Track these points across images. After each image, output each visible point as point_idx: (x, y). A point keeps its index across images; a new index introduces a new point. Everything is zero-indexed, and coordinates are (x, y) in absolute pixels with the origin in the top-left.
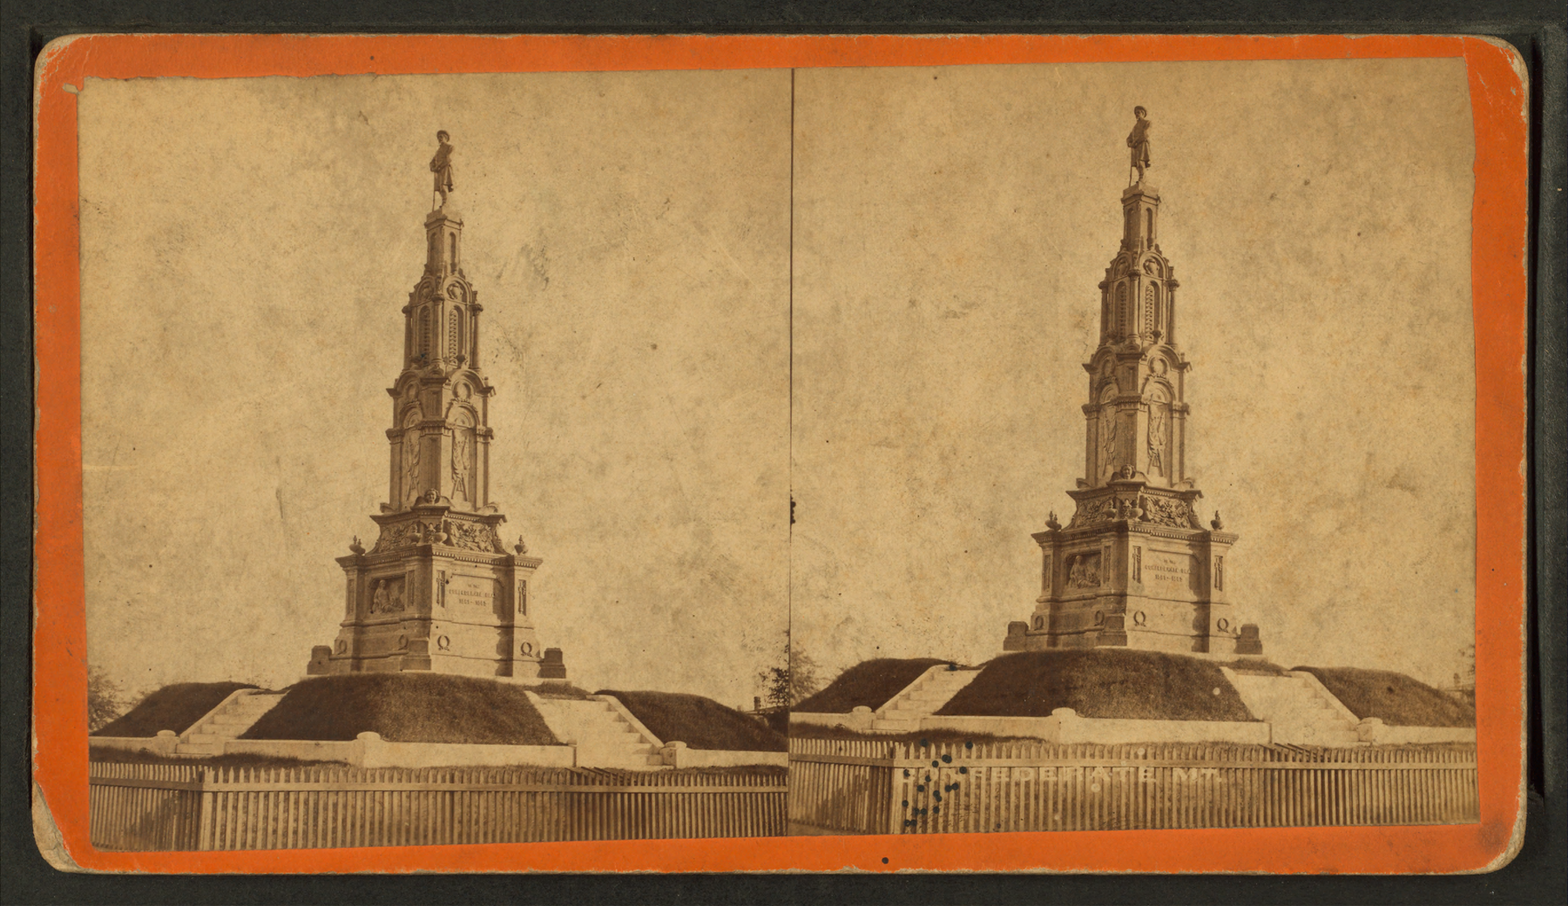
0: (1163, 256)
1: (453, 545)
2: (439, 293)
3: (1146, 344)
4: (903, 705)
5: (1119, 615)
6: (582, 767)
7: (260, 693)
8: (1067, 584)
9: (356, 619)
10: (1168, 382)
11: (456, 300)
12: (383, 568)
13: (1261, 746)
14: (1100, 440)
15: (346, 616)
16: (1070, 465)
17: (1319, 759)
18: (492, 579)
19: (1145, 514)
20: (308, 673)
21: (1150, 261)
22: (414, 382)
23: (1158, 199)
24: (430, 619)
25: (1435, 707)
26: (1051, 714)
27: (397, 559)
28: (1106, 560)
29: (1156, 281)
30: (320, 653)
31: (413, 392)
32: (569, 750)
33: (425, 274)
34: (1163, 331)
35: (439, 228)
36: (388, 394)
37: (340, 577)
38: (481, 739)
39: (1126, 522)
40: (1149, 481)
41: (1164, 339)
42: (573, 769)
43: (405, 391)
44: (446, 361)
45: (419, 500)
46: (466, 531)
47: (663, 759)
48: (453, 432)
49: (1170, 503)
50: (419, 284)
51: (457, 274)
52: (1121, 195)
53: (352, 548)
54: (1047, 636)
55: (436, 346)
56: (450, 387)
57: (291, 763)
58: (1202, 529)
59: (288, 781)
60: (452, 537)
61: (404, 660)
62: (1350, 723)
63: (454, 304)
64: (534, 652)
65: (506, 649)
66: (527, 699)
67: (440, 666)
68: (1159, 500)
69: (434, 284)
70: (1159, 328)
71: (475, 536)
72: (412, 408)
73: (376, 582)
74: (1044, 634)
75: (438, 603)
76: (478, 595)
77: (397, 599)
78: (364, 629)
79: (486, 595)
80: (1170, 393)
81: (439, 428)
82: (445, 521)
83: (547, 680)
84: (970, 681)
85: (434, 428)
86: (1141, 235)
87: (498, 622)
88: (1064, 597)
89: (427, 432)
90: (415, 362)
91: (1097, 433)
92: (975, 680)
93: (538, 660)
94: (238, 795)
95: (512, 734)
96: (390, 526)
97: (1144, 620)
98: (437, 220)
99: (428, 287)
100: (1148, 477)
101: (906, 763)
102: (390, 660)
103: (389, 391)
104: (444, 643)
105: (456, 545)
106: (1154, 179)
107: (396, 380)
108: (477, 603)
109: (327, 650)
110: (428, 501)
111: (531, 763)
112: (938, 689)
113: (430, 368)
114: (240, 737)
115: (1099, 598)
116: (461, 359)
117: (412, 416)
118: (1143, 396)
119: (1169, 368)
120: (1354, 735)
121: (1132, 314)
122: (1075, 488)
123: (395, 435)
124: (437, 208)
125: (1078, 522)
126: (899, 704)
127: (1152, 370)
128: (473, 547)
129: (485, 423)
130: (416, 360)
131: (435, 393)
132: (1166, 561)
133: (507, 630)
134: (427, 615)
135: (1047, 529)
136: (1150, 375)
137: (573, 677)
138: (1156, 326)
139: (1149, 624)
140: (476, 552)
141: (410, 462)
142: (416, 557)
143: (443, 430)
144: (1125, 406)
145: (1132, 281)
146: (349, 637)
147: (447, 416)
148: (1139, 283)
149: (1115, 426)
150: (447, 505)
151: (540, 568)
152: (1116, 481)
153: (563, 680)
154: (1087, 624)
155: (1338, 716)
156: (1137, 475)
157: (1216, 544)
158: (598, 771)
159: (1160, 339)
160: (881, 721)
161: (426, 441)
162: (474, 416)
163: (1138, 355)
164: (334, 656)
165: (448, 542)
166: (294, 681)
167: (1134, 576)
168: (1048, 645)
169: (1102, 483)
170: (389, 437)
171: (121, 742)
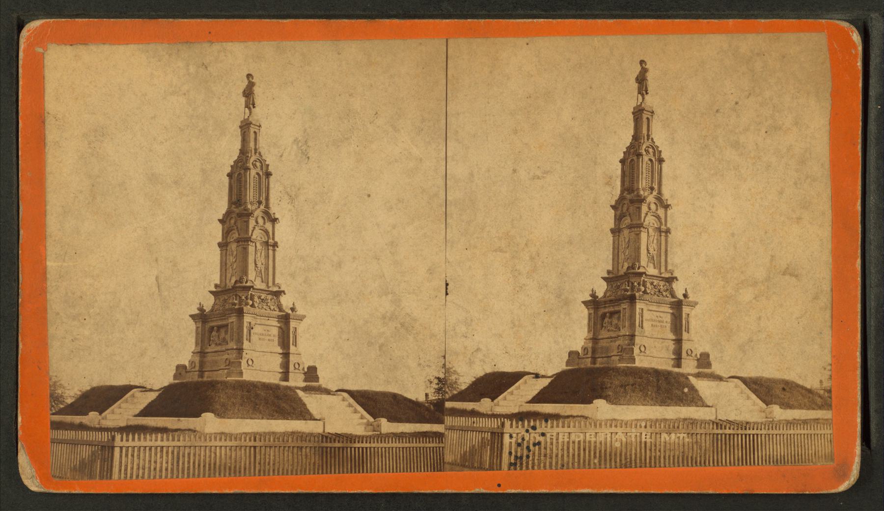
0: (656, 144)
1: (255, 307)
2: (248, 165)
3: (646, 194)
5: (631, 347)
7: (147, 391)
9: (201, 349)
16: (603, 262)
19: (645, 290)
20: (174, 380)
21: (648, 147)
22: (234, 215)
23: (653, 112)
24: (243, 349)
27: (224, 315)
30: (572, 354)
31: (233, 221)
34: (656, 187)
37: (192, 325)
41: (657, 191)
43: (228, 220)
44: (251, 203)
45: (236, 282)
46: (263, 299)
50: (628, 147)
51: (257, 154)
52: (632, 110)
57: (164, 430)
59: (162, 440)
60: (255, 303)
61: (228, 373)
63: (256, 171)
64: (301, 368)
67: (248, 376)
73: (212, 328)
76: (270, 335)
79: (274, 336)
81: (248, 241)
82: (251, 294)
83: (308, 383)
85: (244, 241)
87: (281, 351)
88: (600, 337)
93: (303, 372)
101: (511, 431)
102: (220, 372)
103: (219, 220)
104: (250, 363)
106: (651, 101)
108: (269, 340)
109: (184, 367)
110: (241, 283)
113: (242, 207)
114: (136, 416)
116: (260, 203)
119: (659, 208)
122: (606, 275)
123: (223, 246)
125: (608, 295)
127: (649, 209)
129: (273, 239)
130: (235, 203)
131: (245, 222)
132: (657, 317)
135: (590, 298)
137: (323, 382)
138: (652, 184)
140: (269, 311)
145: (638, 158)
146: (197, 359)
154: (613, 352)
156: (249, 282)
161: (240, 249)
163: (642, 200)
164: (188, 370)
165: (253, 306)
166: (166, 384)
168: (591, 364)
169: (622, 272)
170: (612, 233)
171: (68, 419)
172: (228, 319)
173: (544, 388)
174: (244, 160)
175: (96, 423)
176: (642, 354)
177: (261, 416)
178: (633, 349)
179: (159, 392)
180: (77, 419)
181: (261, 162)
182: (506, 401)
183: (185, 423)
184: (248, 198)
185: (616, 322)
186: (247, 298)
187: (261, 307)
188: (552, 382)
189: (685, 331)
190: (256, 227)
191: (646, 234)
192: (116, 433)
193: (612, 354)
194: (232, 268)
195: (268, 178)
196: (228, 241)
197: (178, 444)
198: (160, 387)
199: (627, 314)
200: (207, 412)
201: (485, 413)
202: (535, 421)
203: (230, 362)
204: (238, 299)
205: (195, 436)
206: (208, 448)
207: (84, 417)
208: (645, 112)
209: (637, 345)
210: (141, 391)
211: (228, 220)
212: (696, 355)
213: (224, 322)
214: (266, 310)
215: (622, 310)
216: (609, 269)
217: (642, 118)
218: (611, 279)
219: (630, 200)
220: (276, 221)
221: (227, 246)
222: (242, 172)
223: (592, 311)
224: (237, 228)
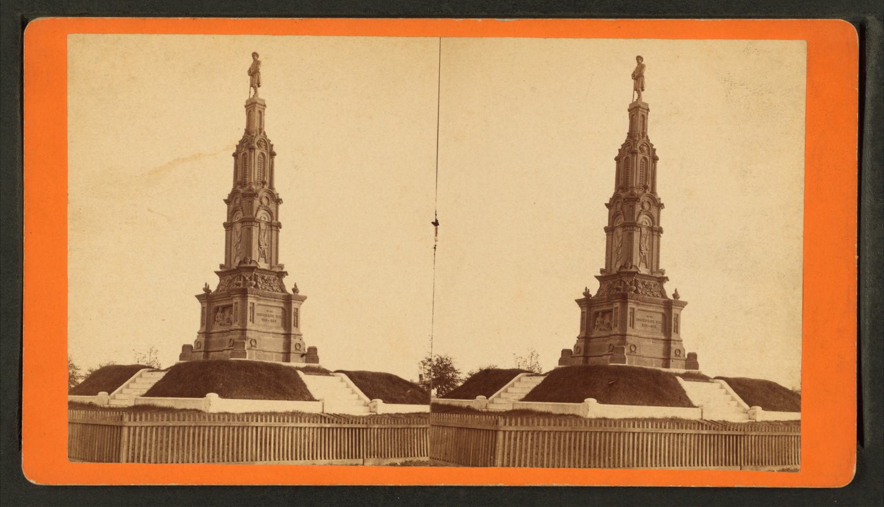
1: (258, 288)
2: (253, 145)
3: (640, 192)
4: (125, 391)
7: (153, 371)
10: (270, 210)
11: (644, 153)
12: (221, 301)
18: (280, 307)
19: (637, 290)
21: (643, 145)
22: (239, 196)
23: (265, 106)
24: (626, 335)
26: (584, 402)
27: (229, 295)
28: (615, 315)
29: (647, 157)
30: (565, 352)
33: (627, 138)
34: (650, 186)
36: (605, 207)
37: (197, 306)
39: (247, 289)
40: (639, 271)
41: (268, 185)
45: (240, 262)
48: (641, 229)
50: (241, 140)
51: (645, 139)
52: (245, 104)
53: (584, 294)
54: (203, 353)
55: (632, 180)
57: (170, 410)
59: (544, 425)
60: (258, 284)
61: (611, 358)
67: (251, 356)
68: (645, 282)
70: (647, 183)
71: (651, 288)
72: (618, 215)
73: (217, 309)
74: (581, 357)
75: (630, 326)
76: (272, 316)
78: (211, 335)
80: (652, 222)
82: (635, 280)
84: (540, 382)
86: (639, 130)
89: (245, 224)
90: (621, 189)
91: (231, 239)
92: (164, 377)
94: (517, 433)
96: (225, 278)
101: (130, 424)
102: (604, 357)
106: (646, 97)
107: (610, 199)
109: (190, 347)
110: (245, 263)
112: (143, 383)
114: (522, 400)
117: (618, 219)
118: (256, 218)
119: (270, 202)
121: (633, 174)
122: (219, 270)
123: (228, 226)
124: (635, 100)
125: (220, 289)
126: (123, 390)
127: (261, 203)
128: (270, 290)
129: (277, 219)
132: (267, 311)
139: (637, 351)
140: (271, 292)
142: (239, 295)
143: (635, 227)
144: (628, 227)
145: (250, 151)
146: (203, 339)
147: (256, 216)
148: (254, 153)
149: (241, 235)
150: (636, 270)
153: (698, 371)
154: (604, 351)
156: (633, 267)
157: (295, 301)
160: (113, 400)
161: (245, 230)
163: (254, 195)
164: (573, 356)
166: (173, 364)
167: (250, 319)
169: (614, 272)
170: (224, 227)
171: (456, 402)
173: (537, 386)
174: (632, 144)
178: (624, 348)
179: (166, 372)
180: (465, 403)
181: (648, 146)
183: (570, 408)
185: (608, 321)
186: (631, 283)
187: (263, 287)
189: (674, 331)
190: (642, 212)
193: (604, 353)
195: (271, 158)
196: (615, 226)
197: (183, 424)
200: (211, 392)
202: (123, 412)
203: (613, 347)
204: (242, 279)
205: (200, 416)
206: (212, 428)
209: (248, 339)
212: (684, 356)
213: (228, 303)
215: (614, 309)
216: (601, 268)
217: (637, 114)
218: (604, 278)
219: (242, 194)
220: (279, 201)
222: (247, 151)
224: (623, 213)
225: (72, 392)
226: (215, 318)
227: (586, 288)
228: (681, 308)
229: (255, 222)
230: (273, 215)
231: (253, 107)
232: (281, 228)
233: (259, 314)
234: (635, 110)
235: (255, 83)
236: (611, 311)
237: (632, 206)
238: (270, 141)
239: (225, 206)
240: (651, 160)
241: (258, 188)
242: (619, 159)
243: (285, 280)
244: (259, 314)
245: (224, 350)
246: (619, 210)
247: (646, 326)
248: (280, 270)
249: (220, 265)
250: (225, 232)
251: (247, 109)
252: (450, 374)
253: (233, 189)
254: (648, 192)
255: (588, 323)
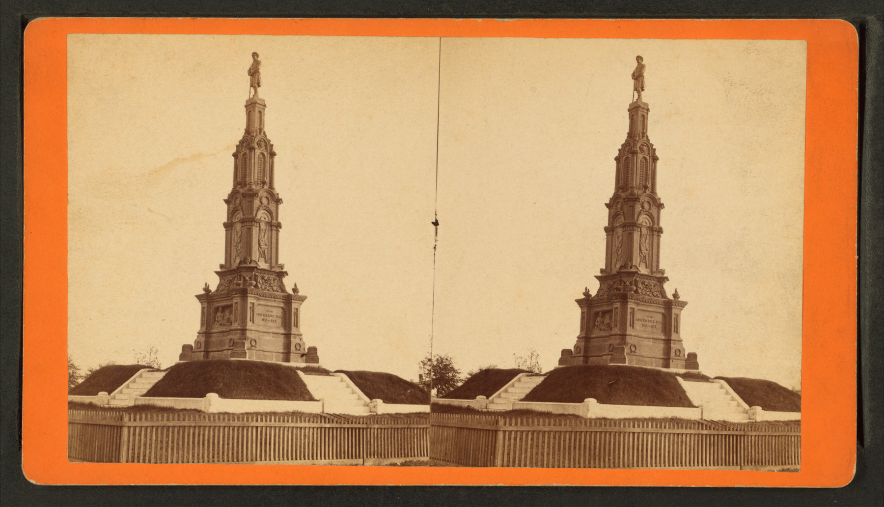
1: (259, 288)
2: (253, 145)
3: (640, 192)
5: (621, 346)
6: (327, 414)
8: (214, 323)
9: (586, 334)
11: (261, 149)
13: (697, 421)
14: (232, 243)
15: (201, 328)
17: (350, 422)
18: (280, 307)
21: (643, 145)
22: (239, 196)
23: (265, 106)
25: (790, 401)
27: (229, 295)
28: (615, 315)
29: (646, 157)
30: (565, 352)
32: (699, 410)
33: (627, 138)
34: (650, 186)
35: (252, 108)
37: (197, 306)
38: (651, 403)
40: (639, 271)
41: (268, 185)
42: (322, 414)
43: (615, 205)
45: (240, 263)
47: (749, 416)
49: (270, 278)
50: (241, 140)
53: (584, 294)
55: (632, 180)
56: (258, 199)
57: (170, 410)
58: (287, 293)
60: (258, 284)
62: (365, 402)
65: (667, 351)
66: (298, 375)
67: (251, 356)
68: (645, 282)
69: (632, 144)
73: (217, 309)
76: (272, 316)
77: (228, 318)
83: (688, 370)
86: (639, 130)
89: (245, 224)
95: (289, 394)
97: (635, 349)
98: (635, 107)
99: (246, 142)
100: (259, 263)
101: (130, 424)
102: (604, 357)
103: (606, 205)
105: (260, 288)
106: (646, 97)
107: (229, 195)
109: (190, 347)
110: (245, 263)
111: (299, 411)
114: (522, 400)
115: (231, 332)
117: (237, 215)
118: (256, 218)
119: (270, 201)
120: (746, 415)
122: (219, 270)
123: (228, 226)
124: (635, 100)
125: (221, 289)
127: (261, 203)
130: (622, 188)
131: (249, 202)
132: (268, 311)
133: (288, 336)
134: (624, 333)
135: (583, 297)
136: (260, 206)
137: (703, 369)
141: (236, 241)
142: (239, 295)
145: (250, 152)
146: (203, 339)
151: (306, 301)
152: (242, 265)
154: (605, 351)
155: (359, 398)
156: (633, 267)
158: (335, 415)
159: (265, 185)
162: (270, 215)
163: (254, 195)
164: (573, 356)
166: (173, 364)
167: (250, 319)
168: (204, 357)
169: (614, 272)
170: (225, 227)
172: (612, 304)
174: (632, 144)
175: (483, 407)
176: (253, 348)
177: (641, 402)
180: (465, 403)
181: (648, 146)
182: (507, 394)
183: (570, 408)
184: (635, 184)
186: (631, 284)
188: (166, 375)
191: (258, 228)
192: (499, 417)
193: (604, 353)
194: (236, 248)
197: (184, 424)
198: (167, 367)
199: (239, 308)
201: (102, 406)
203: (613, 347)
204: (242, 280)
207: (93, 397)
208: (640, 109)
209: (248, 339)
210: (149, 371)
211: (615, 205)
214: (268, 290)
217: (637, 114)
218: (604, 278)
220: (279, 201)
221: (613, 231)
222: (247, 151)
223: (206, 305)
225: (72, 392)
226: (215, 318)
227: (586, 288)
228: (301, 302)
229: (255, 222)
230: (273, 215)
231: (253, 107)
232: (281, 228)
233: (259, 314)
234: (635, 110)
235: (255, 83)
236: (611, 311)
237: (632, 206)
238: (653, 145)
239: (225, 206)
240: (651, 160)
241: (258, 188)
242: (619, 159)
243: (285, 280)
244: (259, 314)
245: (224, 350)
246: (619, 209)
247: (646, 326)
248: (280, 270)
249: (601, 269)
250: (225, 232)
251: (247, 110)
252: (450, 374)
253: (233, 189)
254: (648, 192)
255: (588, 323)
